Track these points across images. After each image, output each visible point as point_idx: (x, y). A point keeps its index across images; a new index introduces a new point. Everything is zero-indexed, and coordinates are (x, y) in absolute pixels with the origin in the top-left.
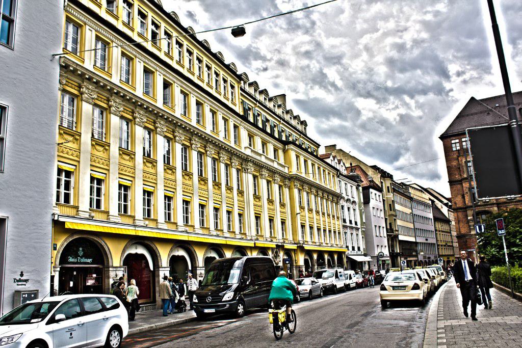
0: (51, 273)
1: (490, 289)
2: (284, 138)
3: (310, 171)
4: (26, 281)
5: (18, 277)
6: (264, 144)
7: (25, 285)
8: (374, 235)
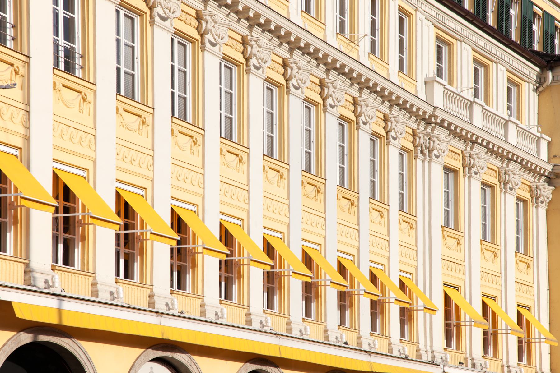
6: (480, 67)
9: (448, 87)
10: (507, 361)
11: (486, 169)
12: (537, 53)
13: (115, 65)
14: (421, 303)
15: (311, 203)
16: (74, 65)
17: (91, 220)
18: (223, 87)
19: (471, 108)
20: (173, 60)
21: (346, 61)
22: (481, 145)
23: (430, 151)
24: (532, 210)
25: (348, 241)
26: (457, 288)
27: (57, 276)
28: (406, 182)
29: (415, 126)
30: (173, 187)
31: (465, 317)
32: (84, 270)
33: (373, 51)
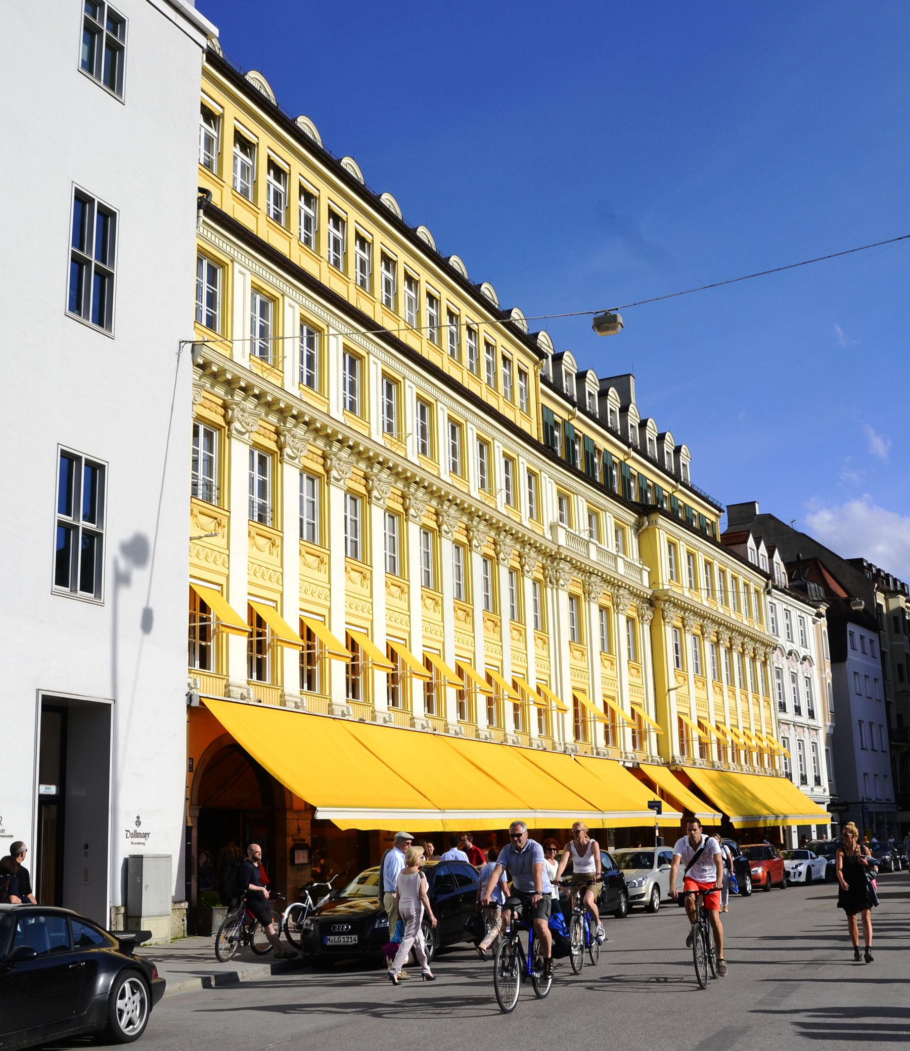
3: (702, 583)
4: (146, 835)
6: (593, 515)
7: (144, 844)
8: (857, 746)
9: (569, 529)
10: (624, 749)
11: (601, 594)
12: (635, 503)
13: (298, 516)
14: (554, 704)
15: (462, 625)
16: (266, 517)
17: (279, 643)
18: (387, 532)
20: (346, 511)
21: (487, 510)
22: (597, 575)
23: (557, 581)
24: (638, 626)
25: (493, 655)
26: (584, 691)
27: (252, 689)
28: (540, 606)
30: (347, 613)
31: (590, 714)
32: (219, 675)
33: (508, 502)
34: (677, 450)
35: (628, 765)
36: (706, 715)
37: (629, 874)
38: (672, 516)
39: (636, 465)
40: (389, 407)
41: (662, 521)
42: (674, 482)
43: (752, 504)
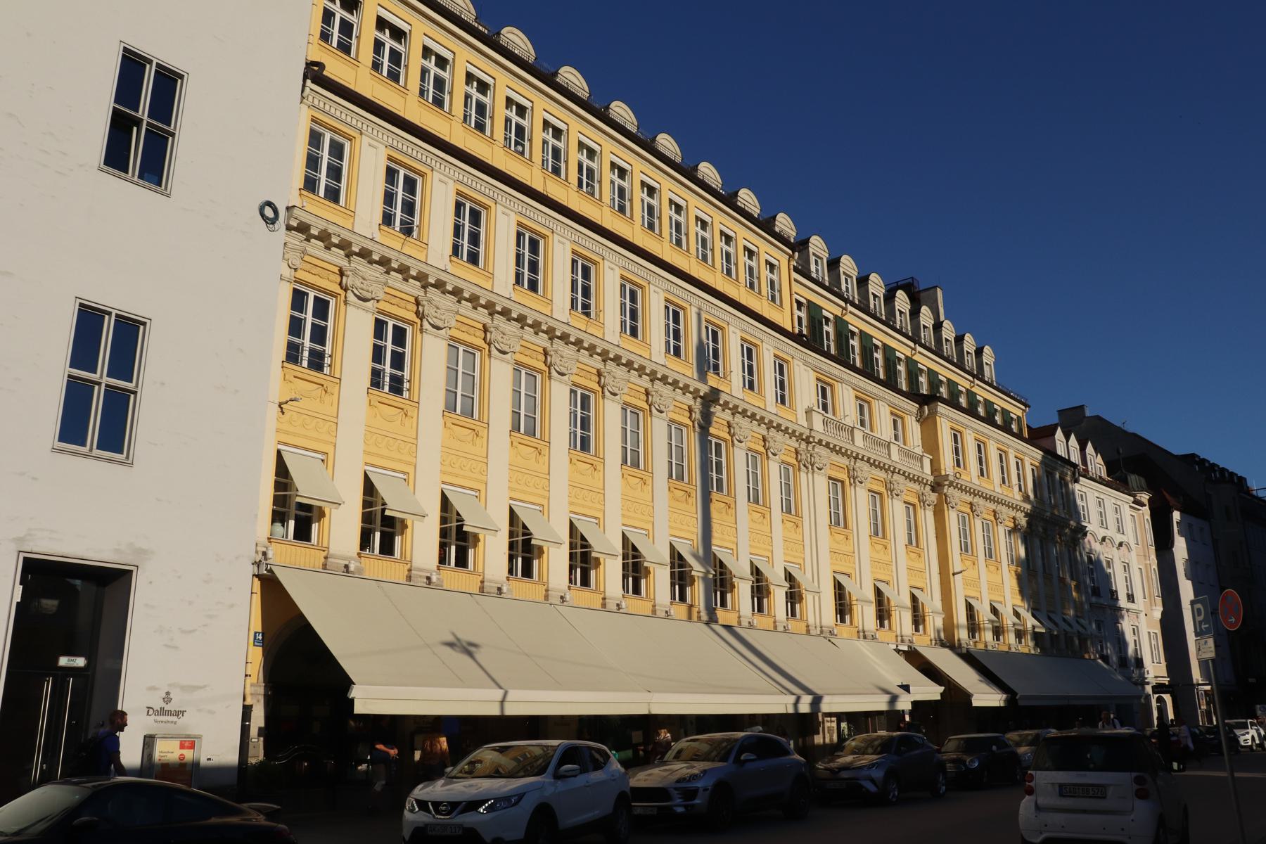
0: (244, 699)
1: (359, 709)
2: (924, 390)
5: (158, 704)
6: (863, 405)
19: (852, 432)
24: (920, 512)
26: (922, 589)
29: (796, 445)
32: (597, 590)
34: (979, 352)
35: (901, 648)
36: (977, 595)
37: (1238, 732)
38: (953, 403)
39: (925, 360)
40: (957, 449)
41: (942, 408)
42: (912, 344)
43: (1081, 408)
